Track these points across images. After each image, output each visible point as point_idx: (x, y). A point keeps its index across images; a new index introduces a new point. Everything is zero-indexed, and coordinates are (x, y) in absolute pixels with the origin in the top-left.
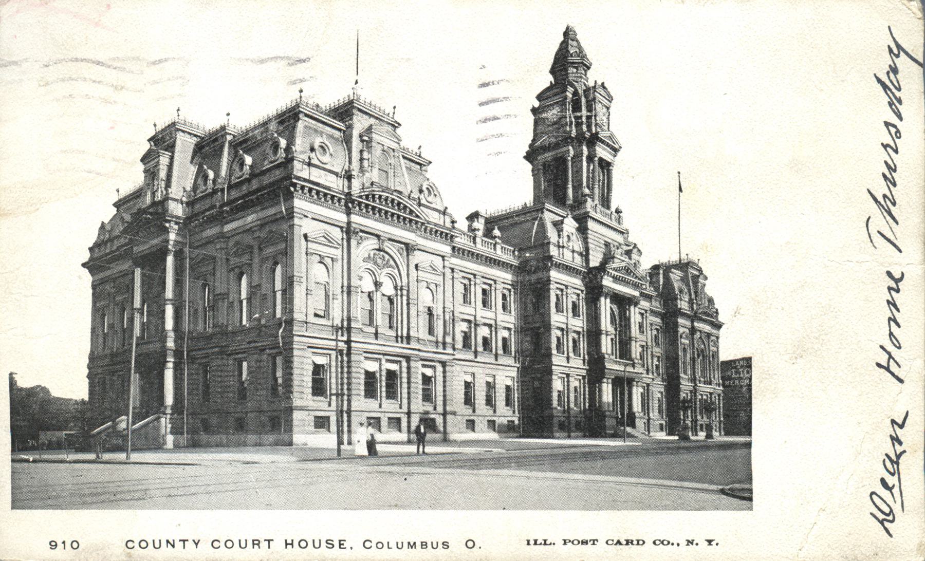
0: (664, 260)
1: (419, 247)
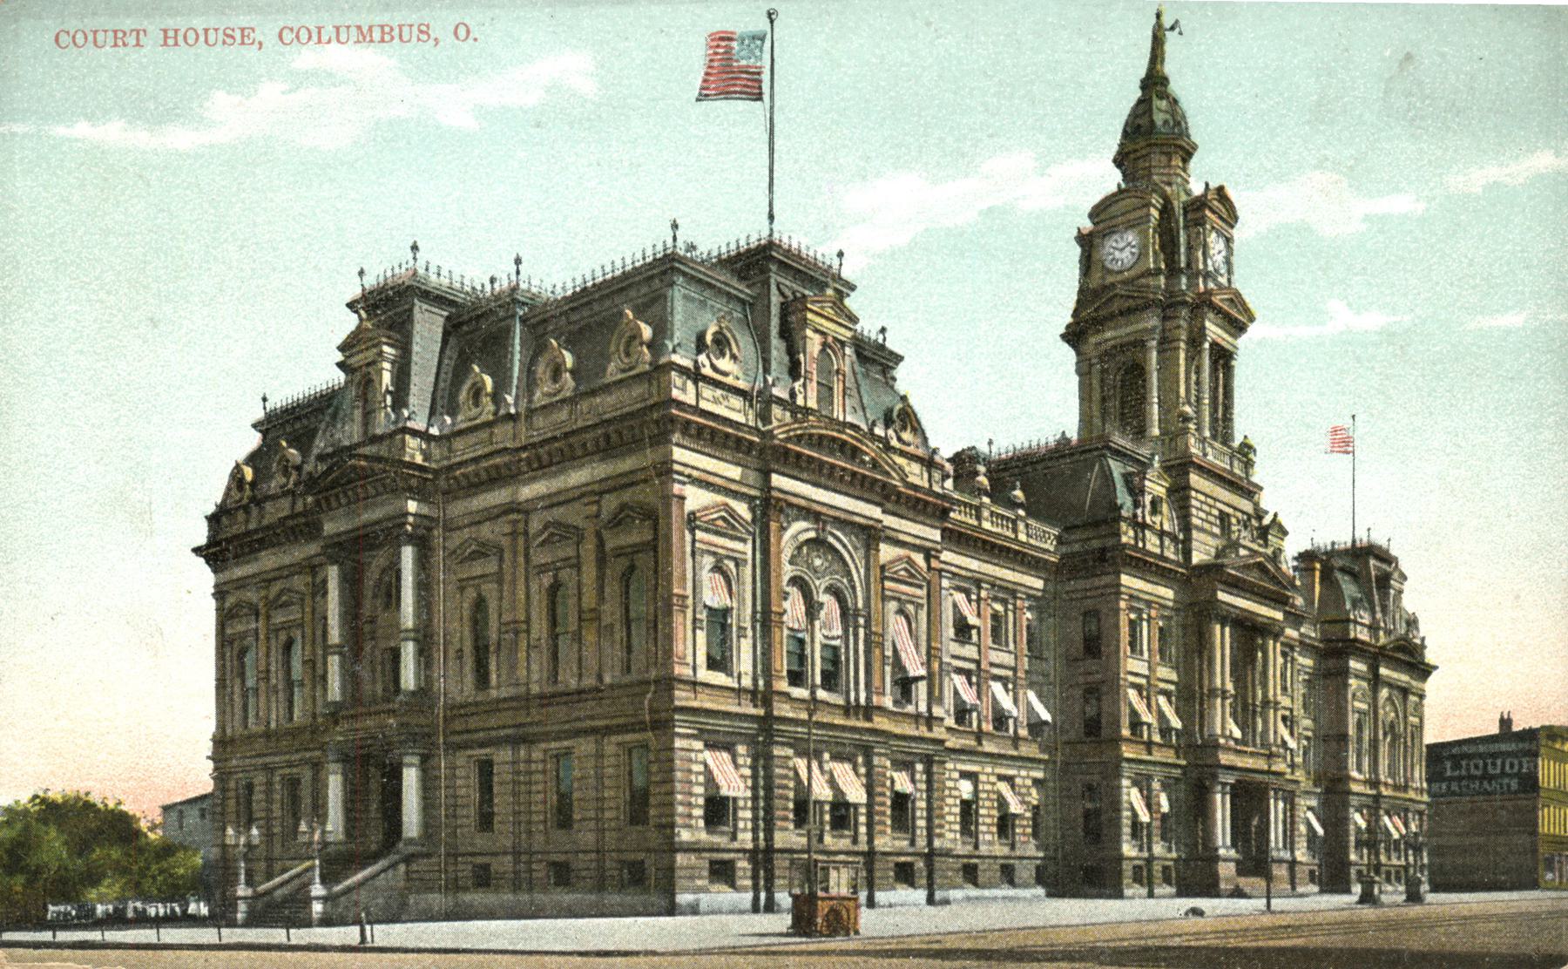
1: (889, 533)
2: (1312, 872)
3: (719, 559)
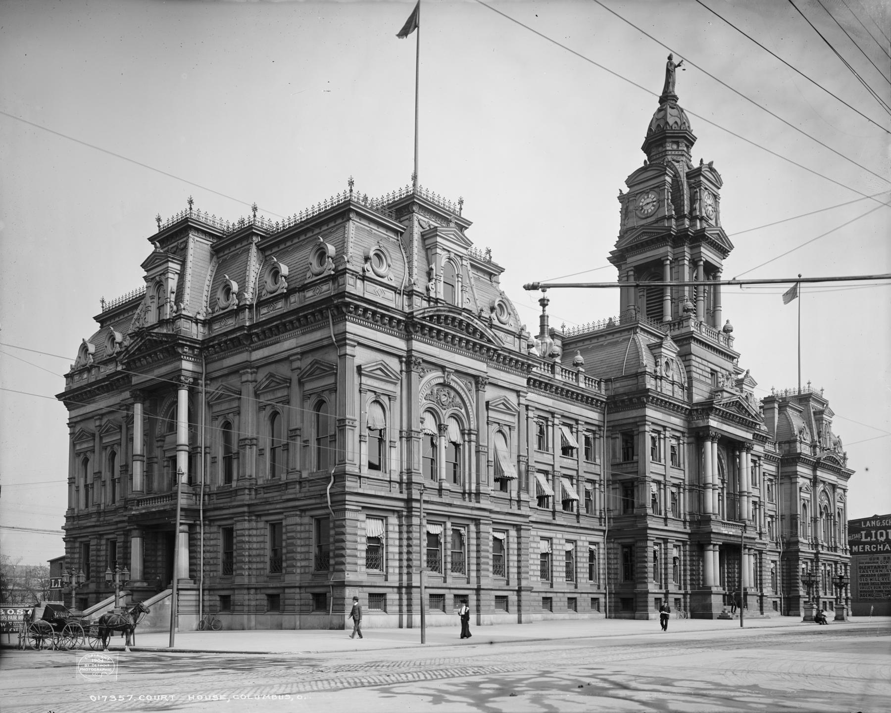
0: (780, 390)
1: (491, 380)
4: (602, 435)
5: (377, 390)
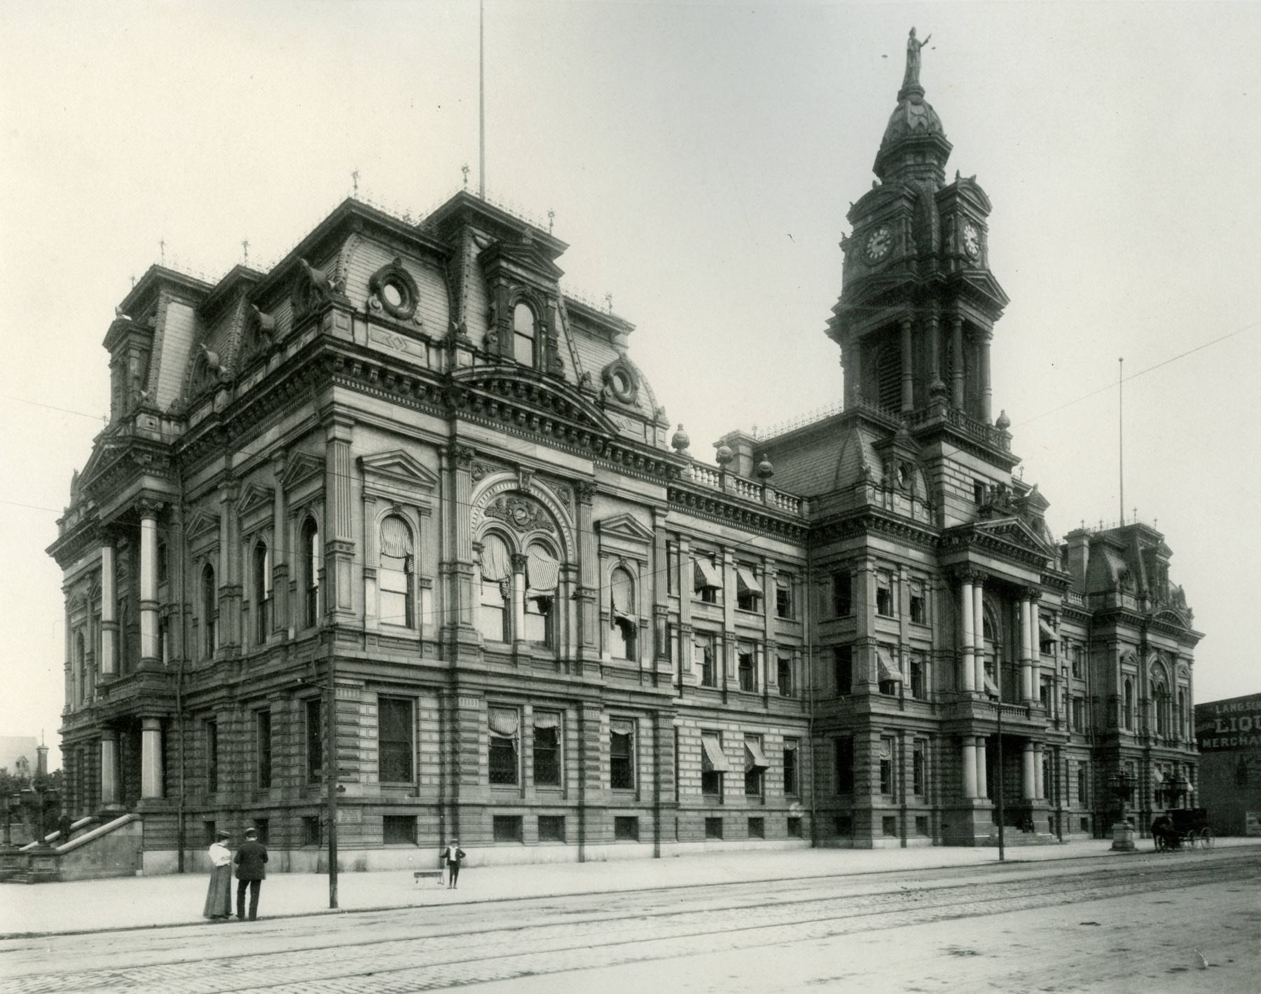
1: (600, 488)
2: (1084, 821)
3: (397, 506)
4: (805, 580)
5: (395, 499)
